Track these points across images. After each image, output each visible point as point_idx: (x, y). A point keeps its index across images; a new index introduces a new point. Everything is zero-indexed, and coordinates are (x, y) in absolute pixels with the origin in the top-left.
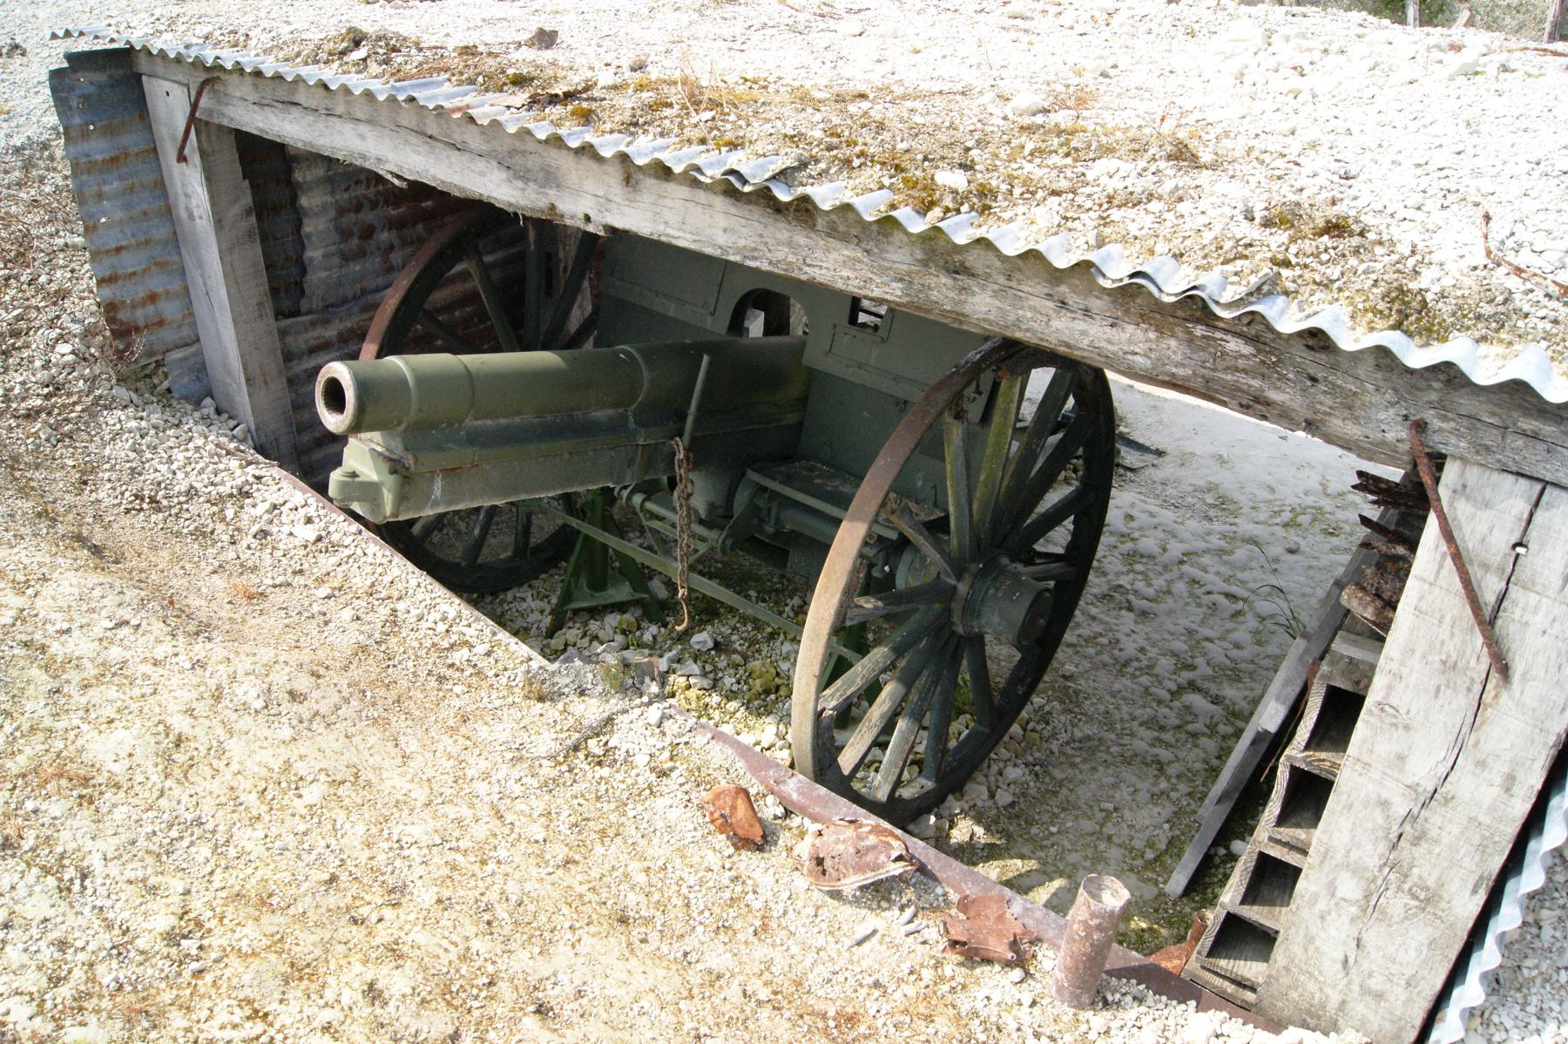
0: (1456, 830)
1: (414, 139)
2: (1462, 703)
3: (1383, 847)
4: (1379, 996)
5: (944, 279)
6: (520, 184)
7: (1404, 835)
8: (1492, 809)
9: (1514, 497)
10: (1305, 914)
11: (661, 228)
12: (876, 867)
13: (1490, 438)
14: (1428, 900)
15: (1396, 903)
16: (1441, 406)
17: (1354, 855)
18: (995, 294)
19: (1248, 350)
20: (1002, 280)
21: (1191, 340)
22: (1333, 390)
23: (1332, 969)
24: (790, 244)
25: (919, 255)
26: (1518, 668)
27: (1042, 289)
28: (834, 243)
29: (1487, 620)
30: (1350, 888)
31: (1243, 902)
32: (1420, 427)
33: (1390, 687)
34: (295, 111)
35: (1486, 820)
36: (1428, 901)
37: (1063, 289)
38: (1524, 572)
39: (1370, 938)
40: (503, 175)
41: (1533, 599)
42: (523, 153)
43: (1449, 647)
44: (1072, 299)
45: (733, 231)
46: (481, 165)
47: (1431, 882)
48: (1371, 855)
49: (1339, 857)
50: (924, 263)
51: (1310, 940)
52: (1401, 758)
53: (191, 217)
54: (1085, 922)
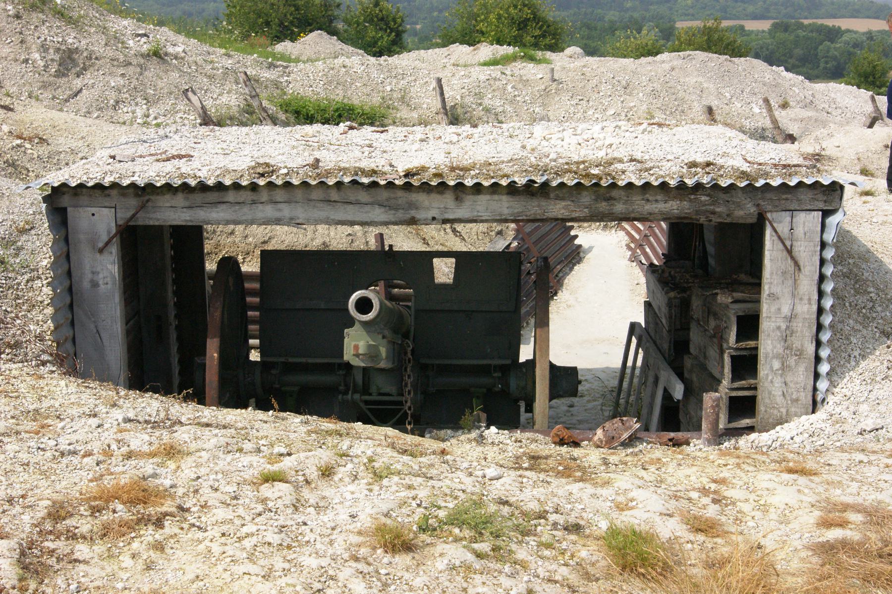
0: (800, 325)
1: (321, 205)
2: (790, 282)
3: (782, 344)
4: (797, 400)
5: (604, 204)
6: (393, 212)
7: (786, 336)
8: (808, 311)
9: (786, 217)
10: (766, 384)
11: (476, 214)
12: (631, 427)
13: (777, 203)
14: (800, 354)
15: (792, 361)
16: (763, 199)
17: (775, 351)
18: (624, 204)
19: (707, 198)
20: (625, 198)
21: (690, 200)
22: (734, 203)
23: (780, 400)
24: (539, 206)
25: (593, 197)
26: (801, 264)
27: (640, 198)
28: (558, 202)
29: (790, 252)
30: (776, 365)
31: (729, 422)
32: (758, 205)
33: (770, 288)
34: (224, 206)
35: (807, 316)
36: (800, 354)
37: (647, 196)
38: (795, 237)
39: (788, 379)
40: (383, 210)
41: (799, 243)
42: (395, 198)
43: (783, 267)
44: (650, 198)
45: (511, 207)
46: (367, 208)
47: (799, 347)
48: (779, 348)
49: (771, 355)
50: (596, 200)
51: (770, 393)
52: (779, 309)
53: (95, 285)
54: (712, 406)
